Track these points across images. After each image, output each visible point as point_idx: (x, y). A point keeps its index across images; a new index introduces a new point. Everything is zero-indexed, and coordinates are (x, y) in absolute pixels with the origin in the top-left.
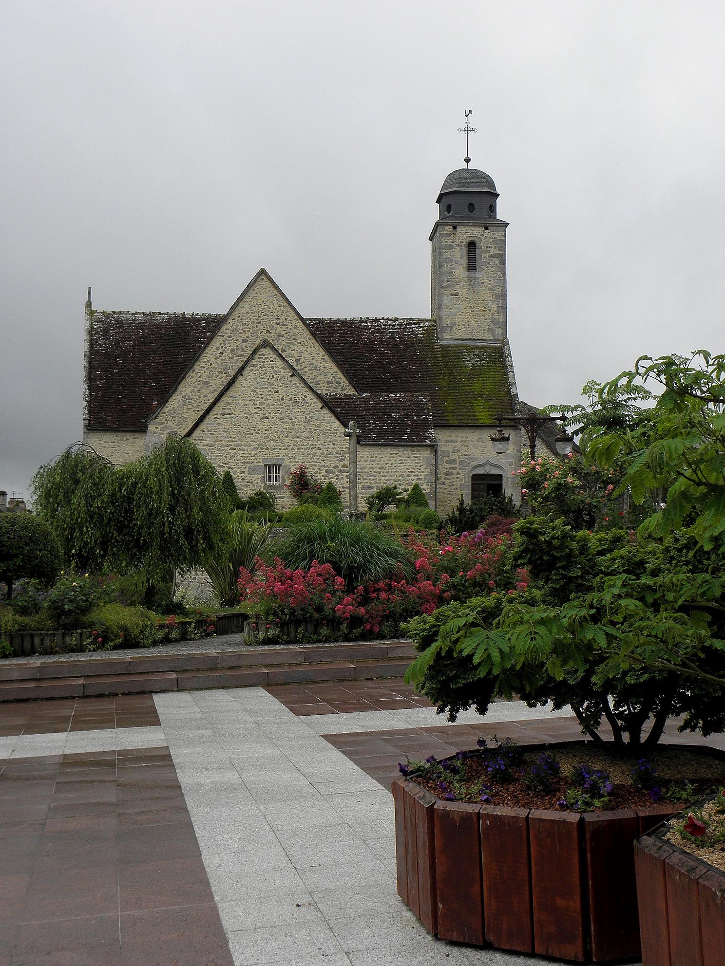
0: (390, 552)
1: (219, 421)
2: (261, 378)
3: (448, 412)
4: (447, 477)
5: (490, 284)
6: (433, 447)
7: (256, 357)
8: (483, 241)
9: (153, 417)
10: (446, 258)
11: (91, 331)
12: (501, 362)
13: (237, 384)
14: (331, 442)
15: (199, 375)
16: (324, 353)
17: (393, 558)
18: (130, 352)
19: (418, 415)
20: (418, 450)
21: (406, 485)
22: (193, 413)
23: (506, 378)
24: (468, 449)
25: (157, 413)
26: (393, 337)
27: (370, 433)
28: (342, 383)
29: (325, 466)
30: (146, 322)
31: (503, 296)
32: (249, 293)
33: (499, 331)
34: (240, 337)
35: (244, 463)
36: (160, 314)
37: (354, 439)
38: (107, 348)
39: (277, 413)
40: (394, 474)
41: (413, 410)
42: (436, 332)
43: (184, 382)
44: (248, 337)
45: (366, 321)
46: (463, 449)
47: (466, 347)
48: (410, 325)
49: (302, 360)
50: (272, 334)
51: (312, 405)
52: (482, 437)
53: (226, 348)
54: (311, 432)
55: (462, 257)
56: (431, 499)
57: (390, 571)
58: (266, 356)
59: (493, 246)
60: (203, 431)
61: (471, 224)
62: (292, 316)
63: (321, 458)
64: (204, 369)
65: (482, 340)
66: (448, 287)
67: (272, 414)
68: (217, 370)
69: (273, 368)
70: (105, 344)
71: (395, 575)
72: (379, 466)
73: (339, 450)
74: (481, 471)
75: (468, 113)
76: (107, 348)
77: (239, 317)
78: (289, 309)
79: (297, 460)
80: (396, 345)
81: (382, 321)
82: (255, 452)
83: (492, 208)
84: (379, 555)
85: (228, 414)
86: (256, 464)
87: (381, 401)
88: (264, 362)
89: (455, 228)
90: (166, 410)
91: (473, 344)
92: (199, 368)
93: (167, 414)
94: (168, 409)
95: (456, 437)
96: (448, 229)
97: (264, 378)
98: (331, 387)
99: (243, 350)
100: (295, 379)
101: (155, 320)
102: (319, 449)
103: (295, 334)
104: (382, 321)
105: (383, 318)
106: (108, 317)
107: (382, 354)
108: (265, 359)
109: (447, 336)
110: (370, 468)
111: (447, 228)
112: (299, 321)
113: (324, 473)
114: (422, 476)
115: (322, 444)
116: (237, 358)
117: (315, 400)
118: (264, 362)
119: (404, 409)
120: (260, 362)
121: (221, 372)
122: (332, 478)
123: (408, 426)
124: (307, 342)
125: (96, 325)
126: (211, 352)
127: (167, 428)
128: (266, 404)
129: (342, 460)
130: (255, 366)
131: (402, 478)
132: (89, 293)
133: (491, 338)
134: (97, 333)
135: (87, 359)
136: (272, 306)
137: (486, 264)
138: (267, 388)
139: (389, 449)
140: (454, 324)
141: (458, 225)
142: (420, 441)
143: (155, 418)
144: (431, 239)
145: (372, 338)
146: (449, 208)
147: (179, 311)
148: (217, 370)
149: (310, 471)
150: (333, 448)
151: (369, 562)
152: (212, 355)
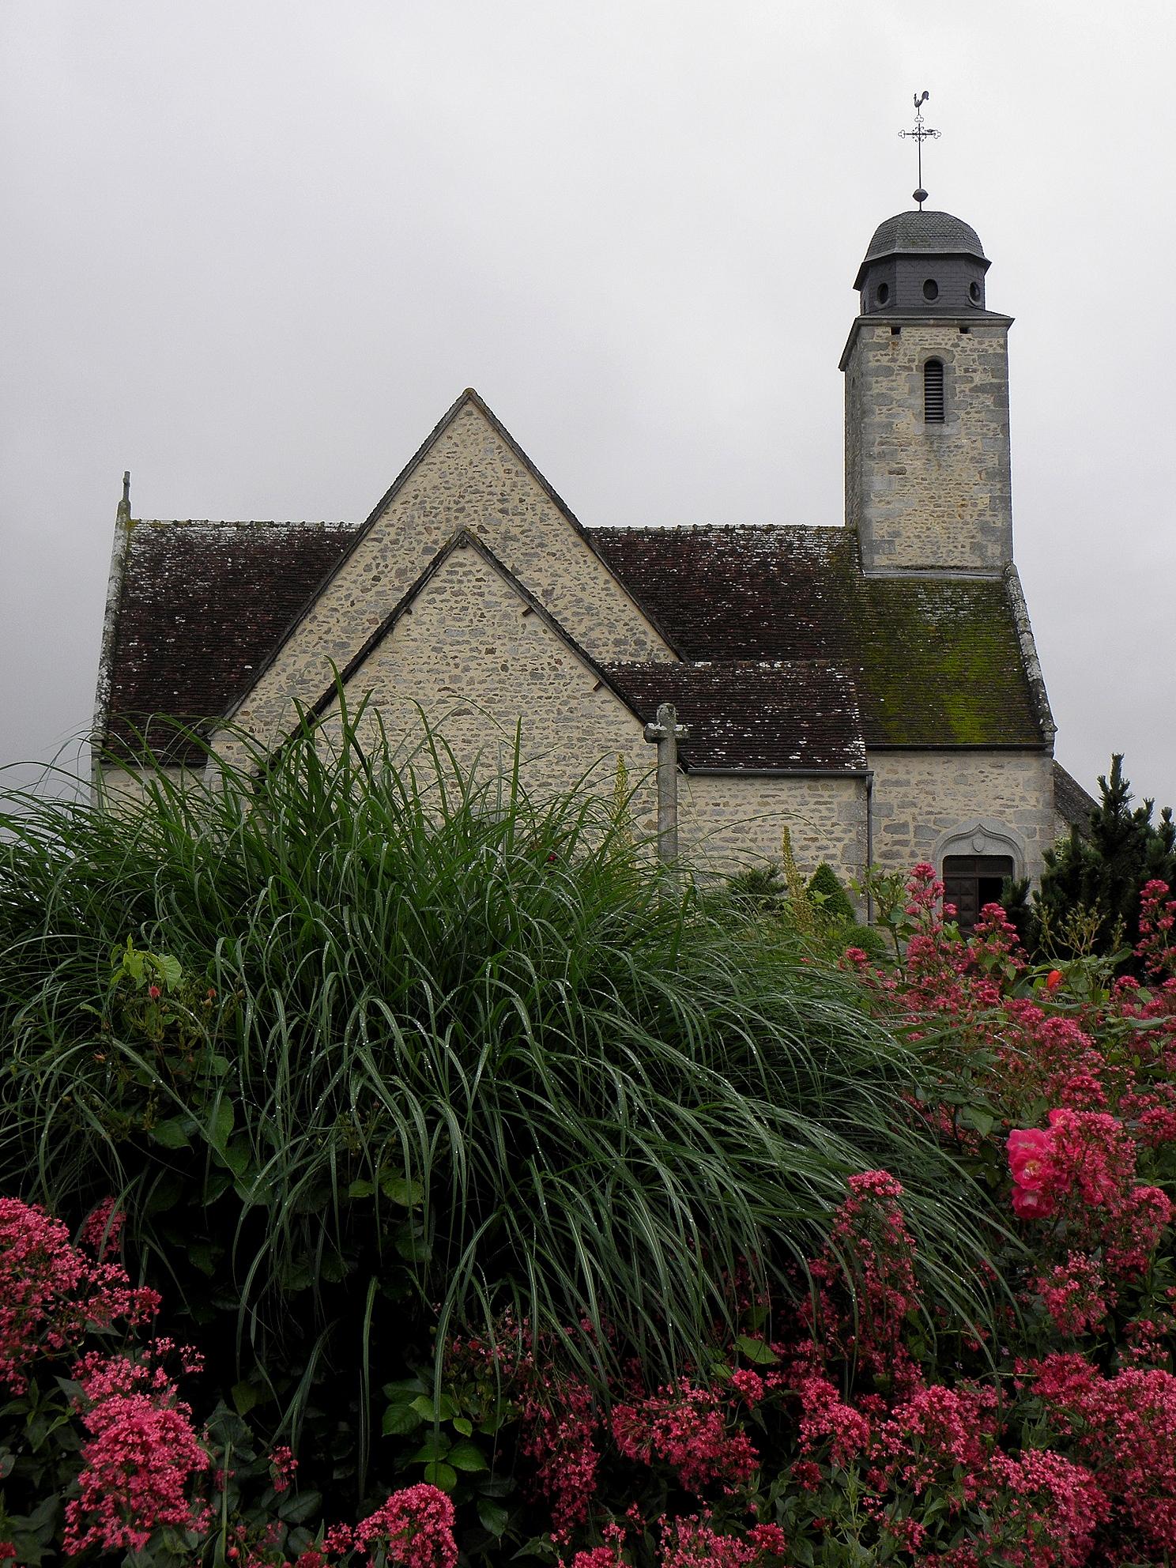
0: (770, 1052)
2: (454, 619)
3: (889, 719)
5: (973, 449)
6: (862, 779)
7: (443, 571)
8: (957, 357)
10: (878, 394)
11: (124, 561)
12: (1002, 613)
13: (399, 631)
15: (325, 627)
16: (607, 577)
17: (810, 1111)
18: (203, 601)
19: (824, 708)
23: (1015, 647)
24: (934, 799)
26: (764, 564)
27: (711, 749)
28: (649, 643)
30: (242, 543)
31: (1003, 474)
32: (439, 444)
34: (419, 542)
36: (272, 524)
37: (670, 750)
38: (156, 594)
40: (769, 844)
41: (813, 698)
42: (858, 552)
43: (291, 643)
45: (706, 533)
46: (924, 800)
47: (923, 584)
48: (801, 539)
49: (558, 592)
52: (965, 772)
53: (386, 566)
54: (572, 746)
55: (912, 391)
56: (858, 903)
57: (779, 1254)
58: (465, 569)
59: (980, 368)
61: (932, 322)
62: (537, 495)
64: (337, 615)
65: (957, 568)
66: (882, 455)
69: (482, 595)
70: (153, 586)
71: (838, 1296)
74: (963, 849)
75: (919, 98)
76: (156, 594)
77: (416, 497)
78: (528, 478)
80: (771, 580)
81: (741, 532)
83: (976, 290)
84: (665, 1078)
87: (738, 678)
88: (460, 582)
89: (896, 331)
90: (249, 706)
91: (940, 577)
92: (325, 612)
94: (255, 704)
95: (908, 773)
96: (883, 333)
97: (461, 620)
98: (624, 652)
100: (535, 623)
101: (261, 538)
103: (543, 534)
104: (741, 532)
105: (743, 527)
106: (162, 533)
107: (741, 599)
108: (465, 574)
109: (880, 560)
111: (879, 331)
112: (552, 504)
114: (837, 849)
117: (581, 670)
118: (460, 582)
119: (792, 696)
120: (451, 581)
123: (802, 733)
124: (569, 550)
125: (137, 549)
126: (353, 577)
128: (465, 679)
130: (440, 591)
132: (127, 485)
133: (978, 564)
134: (138, 564)
135: (111, 615)
136: (489, 473)
137: (964, 405)
138: (468, 642)
140: (897, 534)
141: (904, 325)
142: (830, 765)
144: (843, 366)
145: (718, 566)
146: (883, 292)
147: (312, 518)
151: (562, 1153)
152: (355, 582)
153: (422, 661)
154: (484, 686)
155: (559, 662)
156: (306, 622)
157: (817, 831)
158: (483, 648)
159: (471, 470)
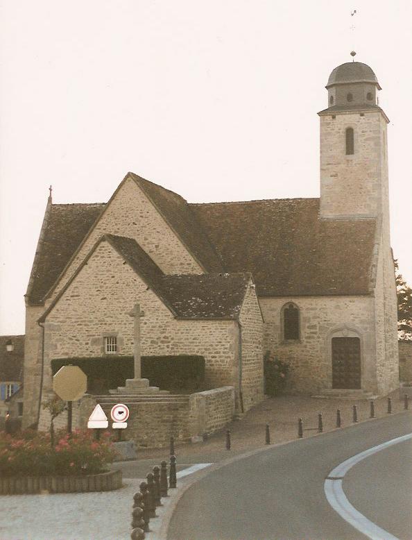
4: (309, 340)
21: (215, 353)
29: (150, 338)
35: (88, 336)
46: (322, 315)
73: (161, 324)
85: (77, 296)
86: (96, 337)
102: (145, 323)
105: (276, 199)
113: (149, 344)
130: (97, 256)
157: (221, 339)
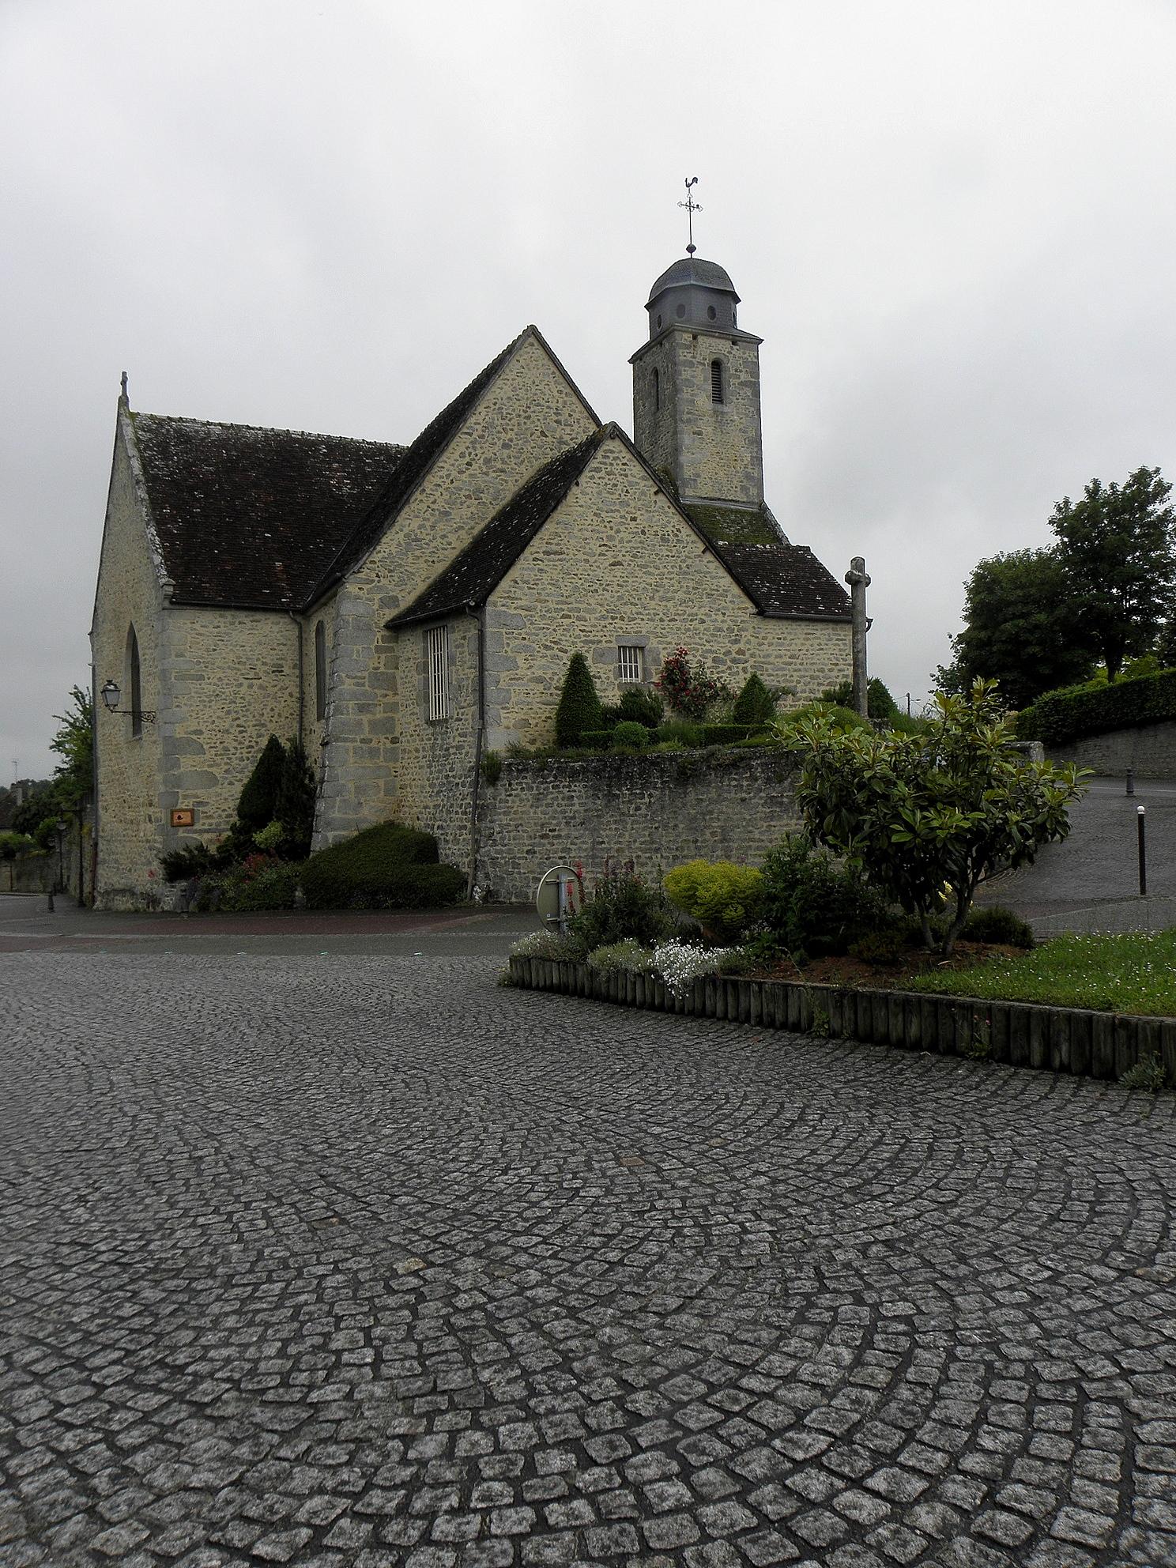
1: (542, 565)
9: (356, 569)
14: (719, 610)
15: (432, 499)
20: (841, 629)
22: (425, 565)
25: (361, 562)
30: (230, 439)
31: (757, 442)
33: (753, 491)
34: (499, 439)
39: (634, 556)
40: (809, 666)
43: (406, 509)
44: (511, 440)
47: (718, 509)
50: (550, 439)
51: (690, 545)
54: (689, 593)
58: (615, 455)
60: (516, 582)
63: (705, 637)
64: (440, 490)
66: (689, 421)
67: (628, 558)
68: (463, 493)
69: (626, 476)
72: (789, 654)
75: (690, 181)
76: (172, 473)
77: (495, 404)
78: (574, 399)
79: (668, 639)
82: (603, 623)
85: (556, 553)
86: (604, 645)
90: (376, 557)
93: (379, 564)
99: (504, 462)
102: (703, 622)
108: (614, 459)
110: (776, 657)
111: (685, 336)
115: (706, 614)
116: (494, 475)
120: (605, 464)
121: (468, 497)
122: (723, 672)
127: (380, 589)
128: (618, 539)
129: (736, 641)
131: (821, 674)
132: (124, 383)
134: (147, 448)
136: (547, 392)
139: (803, 624)
143: (359, 572)
147: (281, 426)
148: (463, 493)
149: (692, 663)
150: (722, 622)
153: (587, 523)
154: (631, 544)
155: (678, 530)
156: (417, 493)
158: (628, 516)
159: (534, 388)
